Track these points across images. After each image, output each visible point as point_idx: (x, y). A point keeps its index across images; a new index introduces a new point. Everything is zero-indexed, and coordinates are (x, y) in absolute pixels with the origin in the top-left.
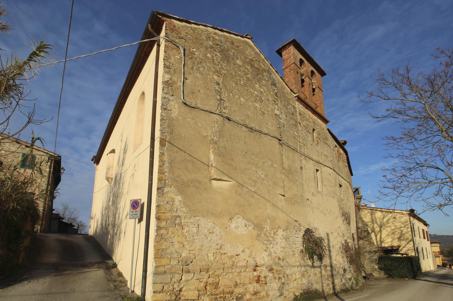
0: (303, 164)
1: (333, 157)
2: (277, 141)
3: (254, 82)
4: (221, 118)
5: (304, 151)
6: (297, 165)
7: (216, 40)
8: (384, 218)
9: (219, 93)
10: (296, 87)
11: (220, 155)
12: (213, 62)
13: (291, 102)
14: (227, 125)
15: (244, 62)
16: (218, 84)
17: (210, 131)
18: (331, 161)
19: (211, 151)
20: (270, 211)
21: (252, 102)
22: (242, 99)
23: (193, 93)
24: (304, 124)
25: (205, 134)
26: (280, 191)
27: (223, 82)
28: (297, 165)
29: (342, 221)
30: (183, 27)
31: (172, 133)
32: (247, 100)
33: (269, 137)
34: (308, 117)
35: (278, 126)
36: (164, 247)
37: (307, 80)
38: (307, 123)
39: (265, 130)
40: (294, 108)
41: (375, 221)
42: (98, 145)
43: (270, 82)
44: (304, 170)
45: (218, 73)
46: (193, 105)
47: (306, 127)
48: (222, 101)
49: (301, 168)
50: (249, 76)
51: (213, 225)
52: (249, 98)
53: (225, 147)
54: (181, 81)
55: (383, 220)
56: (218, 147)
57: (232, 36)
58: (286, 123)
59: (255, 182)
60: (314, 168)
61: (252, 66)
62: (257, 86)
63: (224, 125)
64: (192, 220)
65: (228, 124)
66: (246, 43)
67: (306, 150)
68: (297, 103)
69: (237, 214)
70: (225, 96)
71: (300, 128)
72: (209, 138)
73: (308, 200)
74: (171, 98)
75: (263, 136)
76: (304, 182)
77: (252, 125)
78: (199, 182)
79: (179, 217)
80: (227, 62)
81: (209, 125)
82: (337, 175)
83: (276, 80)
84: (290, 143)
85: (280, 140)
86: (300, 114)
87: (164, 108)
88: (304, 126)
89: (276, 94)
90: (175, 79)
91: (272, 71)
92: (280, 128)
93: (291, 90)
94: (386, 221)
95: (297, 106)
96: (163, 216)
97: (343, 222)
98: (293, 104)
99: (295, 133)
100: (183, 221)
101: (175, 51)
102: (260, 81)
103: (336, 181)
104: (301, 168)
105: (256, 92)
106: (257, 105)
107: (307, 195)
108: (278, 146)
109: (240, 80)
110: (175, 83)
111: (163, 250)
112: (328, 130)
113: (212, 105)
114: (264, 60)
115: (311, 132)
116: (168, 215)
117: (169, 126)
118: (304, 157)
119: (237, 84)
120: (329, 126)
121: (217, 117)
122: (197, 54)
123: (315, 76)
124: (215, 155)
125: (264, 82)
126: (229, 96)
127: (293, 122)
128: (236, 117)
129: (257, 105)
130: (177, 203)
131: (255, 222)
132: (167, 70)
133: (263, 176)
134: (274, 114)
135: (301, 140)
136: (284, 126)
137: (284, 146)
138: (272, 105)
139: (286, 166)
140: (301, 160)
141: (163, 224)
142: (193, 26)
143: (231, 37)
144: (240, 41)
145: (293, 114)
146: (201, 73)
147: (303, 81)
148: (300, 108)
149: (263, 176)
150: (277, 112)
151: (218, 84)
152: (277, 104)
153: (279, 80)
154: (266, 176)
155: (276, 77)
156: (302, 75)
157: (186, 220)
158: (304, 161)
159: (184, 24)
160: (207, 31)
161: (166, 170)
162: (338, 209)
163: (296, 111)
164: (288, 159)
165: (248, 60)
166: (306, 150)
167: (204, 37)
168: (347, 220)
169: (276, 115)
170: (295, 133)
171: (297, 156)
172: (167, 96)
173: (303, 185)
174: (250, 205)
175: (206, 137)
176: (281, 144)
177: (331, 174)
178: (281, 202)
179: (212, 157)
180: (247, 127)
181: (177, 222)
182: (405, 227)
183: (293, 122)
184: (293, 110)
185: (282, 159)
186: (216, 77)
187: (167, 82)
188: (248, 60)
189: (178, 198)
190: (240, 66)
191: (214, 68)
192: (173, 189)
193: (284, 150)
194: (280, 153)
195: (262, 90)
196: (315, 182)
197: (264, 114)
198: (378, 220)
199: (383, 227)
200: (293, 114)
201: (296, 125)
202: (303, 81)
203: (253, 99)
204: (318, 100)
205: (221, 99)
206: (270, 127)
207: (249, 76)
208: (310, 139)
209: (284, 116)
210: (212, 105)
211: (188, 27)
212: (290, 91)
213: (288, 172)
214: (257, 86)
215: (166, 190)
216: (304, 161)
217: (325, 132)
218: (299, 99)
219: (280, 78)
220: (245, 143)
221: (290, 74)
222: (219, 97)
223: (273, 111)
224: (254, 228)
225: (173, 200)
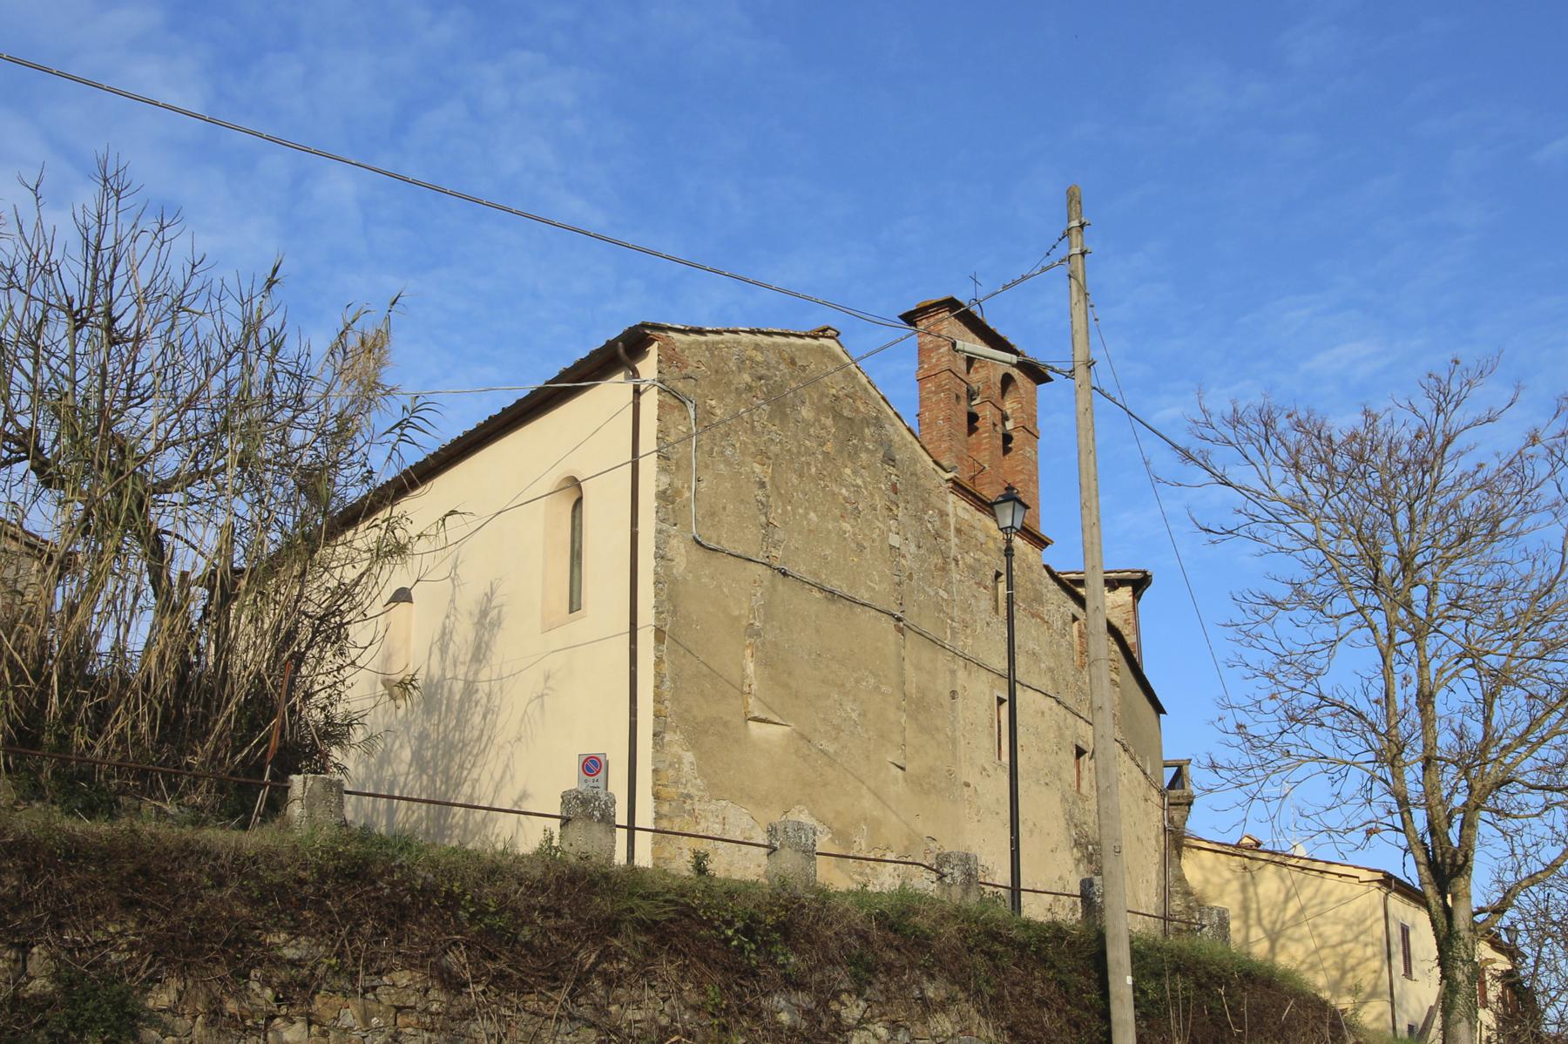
0: (959, 682)
1: (1056, 655)
2: (893, 622)
3: (839, 462)
4: (769, 572)
5: (965, 645)
6: (942, 686)
7: (758, 363)
8: (1287, 900)
9: (764, 506)
10: (950, 449)
11: (765, 662)
12: (753, 427)
13: (934, 499)
14: (780, 587)
15: (820, 410)
16: (762, 485)
17: (746, 605)
18: (1051, 670)
19: (749, 651)
20: (867, 802)
21: (835, 520)
22: (812, 515)
23: (713, 514)
24: (969, 560)
25: (736, 613)
26: (894, 756)
27: (772, 478)
28: (942, 686)
29: (1071, 863)
30: (690, 346)
31: (674, 613)
32: (822, 516)
33: (873, 613)
34: (981, 537)
35: (897, 579)
36: (666, 855)
37: (987, 414)
38: (979, 555)
39: (864, 595)
40: (943, 514)
41: (1253, 915)
42: (1020, 730)
43: (880, 455)
44: (959, 699)
45: (763, 455)
46: (713, 545)
47: (973, 570)
48: (770, 528)
49: (953, 694)
50: (829, 447)
51: (751, 822)
52: (829, 510)
53: (776, 645)
54: (690, 488)
55: (1284, 909)
56: (763, 644)
57: (793, 340)
58: (916, 566)
59: (838, 728)
60: (992, 693)
61: (837, 416)
62: (848, 471)
63: (774, 587)
64: (712, 807)
65: (782, 586)
66: (824, 351)
67: (970, 641)
68: (952, 498)
69: (799, 803)
70: (775, 514)
71: (956, 576)
72: (744, 623)
73: (968, 785)
74: (673, 530)
75: (858, 609)
76: (958, 734)
77: (834, 583)
78: (726, 724)
79: (689, 796)
80: (781, 421)
81: (743, 590)
82: (1069, 716)
83: (897, 439)
84: (926, 626)
85: (899, 619)
86: (959, 531)
87: (660, 556)
88: (970, 567)
89: (895, 490)
90: (678, 484)
91: (888, 416)
92: (900, 584)
93: (936, 463)
94: (1294, 917)
95: (950, 509)
96: (664, 792)
97: (1077, 866)
98: (940, 504)
99: (941, 592)
100: (697, 806)
101: (676, 413)
102: (853, 455)
103: (1061, 736)
104: (953, 694)
105: (844, 491)
106: (846, 526)
107: (967, 773)
108: (892, 636)
109: (809, 464)
110: (678, 493)
111: (665, 860)
112: (1047, 568)
113: (747, 540)
114: (866, 390)
115: (989, 583)
116: (672, 790)
117: (670, 598)
118: (961, 662)
119: (801, 476)
120: (1048, 556)
121: (760, 569)
122: (718, 412)
123: (1017, 388)
124: (758, 663)
125: (863, 456)
126: (785, 512)
127: (937, 560)
128: (799, 568)
129: (846, 526)
130: (686, 767)
131: (836, 825)
132: (664, 463)
133: (854, 716)
134: (886, 547)
135: (956, 613)
136: (910, 577)
137: (909, 634)
138: (884, 522)
139: (911, 689)
140: (953, 672)
141: (665, 808)
142: (711, 337)
143: (790, 345)
144: (810, 349)
145: (937, 535)
146: (728, 463)
147: (973, 418)
148: (960, 512)
149: (854, 716)
150: (895, 540)
151: (762, 485)
152: (895, 518)
153: (903, 438)
154: (863, 714)
155: (896, 431)
156: (971, 395)
157: (703, 806)
158: (961, 674)
159: (693, 337)
160: (739, 343)
161: (667, 695)
162: (1063, 823)
163: (946, 525)
164: (918, 668)
165: (827, 401)
166: (970, 641)
167: (732, 365)
168: (1090, 862)
169: (892, 547)
170: (941, 592)
171: (942, 659)
172: (665, 526)
173: (954, 742)
174: (825, 785)
175: (737, 619)
176: (900, 630)
177: (1047, 712)
178: (896, 785)
179: (751, 667)
180: (822, 589)
181: (687, 807)
182: (1356, 938)
183: (937, 560)
184: (938, 524)
185: (901, 672)
186: (757, 468)
187: (664, 492)
188: (827, 401)
189: (689, 757)
190: (808, 425)
191: (755, 444)
192: (677, 737)
193: (908, 646)
194: (899, 655)
195: (859, 482)
196: (992, 735)
197: (861, 548)
198: (1265, 912)
199: (1282, 941)
200: (937, 535)
201: (943, 569)
202: (973, 418)
203: (837, 512)
204: (1021, 472)
205: (768, 524)
206: (875, 585)
207: (829, 447)
208: (985, 603)
209: (913, 548)
210: (747, 540)
211: (700, 344)
212: (932, 465)
213: (917, 705)
214: (848, 471)
215: (667, 738)
216: (961, 674)
217: (1035, 576)
218: (958, 487)
219: (906, 433)
220: (818, 631)
221: (937, 403)
222: (763, 519)
223: (884, 539)
224: (832, 840)
225: (680, 762)
